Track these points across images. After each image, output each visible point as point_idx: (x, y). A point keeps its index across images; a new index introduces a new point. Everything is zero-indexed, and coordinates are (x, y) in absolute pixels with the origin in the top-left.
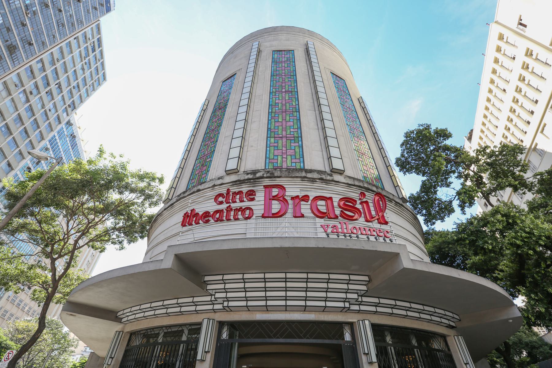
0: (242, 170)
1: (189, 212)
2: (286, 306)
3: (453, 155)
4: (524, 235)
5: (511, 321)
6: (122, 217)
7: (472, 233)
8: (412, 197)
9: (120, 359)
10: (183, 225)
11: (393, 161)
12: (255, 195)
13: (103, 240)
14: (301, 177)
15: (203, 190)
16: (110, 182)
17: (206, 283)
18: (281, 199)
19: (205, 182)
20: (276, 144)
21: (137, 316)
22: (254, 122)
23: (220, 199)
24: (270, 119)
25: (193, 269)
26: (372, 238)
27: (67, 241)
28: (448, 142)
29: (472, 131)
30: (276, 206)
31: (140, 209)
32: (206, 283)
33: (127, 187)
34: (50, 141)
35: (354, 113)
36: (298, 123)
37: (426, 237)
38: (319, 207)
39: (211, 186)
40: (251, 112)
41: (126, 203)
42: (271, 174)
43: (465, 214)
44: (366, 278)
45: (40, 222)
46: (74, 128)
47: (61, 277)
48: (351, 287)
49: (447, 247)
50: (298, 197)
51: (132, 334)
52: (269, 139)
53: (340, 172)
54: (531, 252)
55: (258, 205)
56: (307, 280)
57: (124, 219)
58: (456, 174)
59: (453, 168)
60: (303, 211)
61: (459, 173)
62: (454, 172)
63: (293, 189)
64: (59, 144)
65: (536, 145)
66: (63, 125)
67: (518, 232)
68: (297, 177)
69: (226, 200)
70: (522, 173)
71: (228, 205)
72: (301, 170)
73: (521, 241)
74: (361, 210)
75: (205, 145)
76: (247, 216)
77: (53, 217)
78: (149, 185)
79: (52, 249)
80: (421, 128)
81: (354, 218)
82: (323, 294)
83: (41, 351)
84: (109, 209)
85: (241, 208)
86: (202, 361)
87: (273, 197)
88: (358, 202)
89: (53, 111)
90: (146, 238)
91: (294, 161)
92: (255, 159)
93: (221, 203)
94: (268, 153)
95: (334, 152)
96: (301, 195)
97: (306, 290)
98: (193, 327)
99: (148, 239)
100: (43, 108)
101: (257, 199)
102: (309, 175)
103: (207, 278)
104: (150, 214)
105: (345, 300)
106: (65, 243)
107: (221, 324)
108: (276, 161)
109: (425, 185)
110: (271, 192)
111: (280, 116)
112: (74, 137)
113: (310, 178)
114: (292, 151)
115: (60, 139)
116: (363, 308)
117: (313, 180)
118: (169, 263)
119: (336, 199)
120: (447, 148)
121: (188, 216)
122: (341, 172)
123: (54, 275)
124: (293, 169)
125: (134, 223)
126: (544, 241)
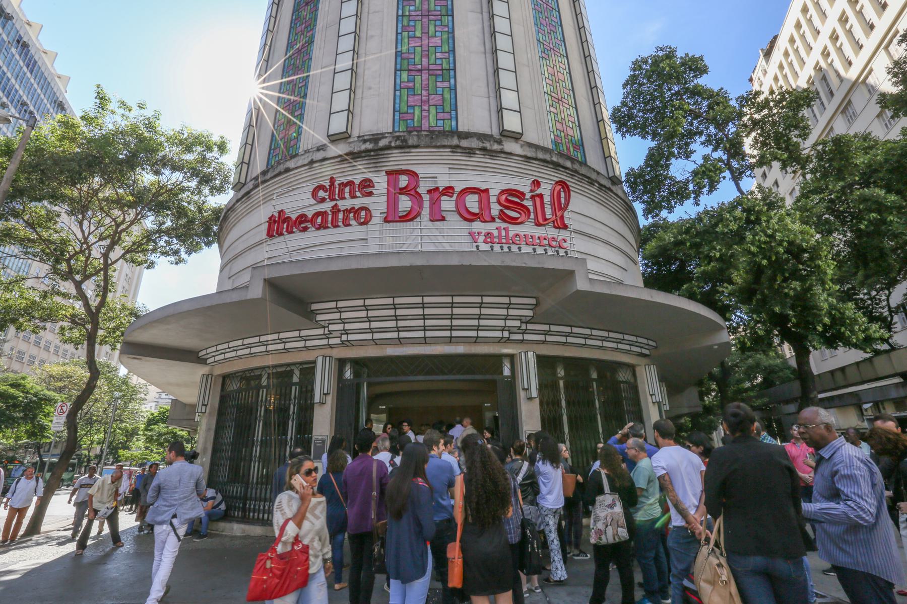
0: (355, 133)
1: (276, 215)
2: (425, 338)
3: (705, 103)
4: (763, 238)
6: (169, 212)
7: (698, 234)
9: (217, 405)
10: (270, 234)
11: (607, 114)
12: (373, 187)
13: (147, 250)
14: (450, 147)
15: (297, 168)
17: (314, 313)
18: (412, 192)
19: (296, 155)
20: (411, 84)
21: (227, 355)
22: (372, 36)
23: (321, 194)
24: (400, 31)
25: (293, 297)
26: (540, 250)
27: (90, 254)
28: (703, 81)
29: (775, 38)
30: (405, 203)
31: (196, 198)
32: (314, 313)
33: (165, 162)
35: (555, 14)
36: (451, 41)
37: (643, 238)
38: (468, 205)
39: (306, 162)
40: (365, 15)
41: (171, 190)
42: (402, 141)
43: (698, 205)
44: (533, 301)
45: (31, 225)
46: (18, 26)
47: (98, 309)
48: (511, 312)
50: (437, 188)
51: (225, 378)
52: (398, 73)
53: (515, 135)
54: (765, 262)
55: (377, 204)
57: (173, 214)
58: (703, 138)
59: (701, 128)
61: (709, 135)
62: (700, 134)
63: (435, 169)
65: (871, 71)
67: (757, 234)
68: (444, 147)
69: (329, 196)
70: (800, 140)
71: (333, 203)
73: (758, 247)
76: (362, 220)
77: (51, 217)
78: (204, 158)
79: (69, 266)
80: (661, 53)
81: (519, 220)
82: (475, 322)
83: (96, 400)
85: (353, 208)
86: (322, 403)
87: (401, 189)
88: (528, 196)
90: (215, 246)
91: (441, 115)
92: (376, 117)
93: (323, 200)
94: (397, 101)
95: (509, 99)
97: (452, 317)
98: (305, 366)
99: (221, 247)
102: (464, 143)
103: (314, 307)
104: (215, 206)
105: (503, 329)
106: (87, 258)
107: (342, 363)
108: (410, 117)
109: (653, 155)
110: (396, 181)
111: (419, 24)
112: (25, 46)
113: (465, 148)
114: (438, 98)
116: (527, 337)
117: (470, 152)
118: (257, 291)
119: (494, 193)
120: (696, 92)
121: (275, 221)
122: (516, 137)
123: (87, 305)
124: (439, 132)
125: (191, 221)
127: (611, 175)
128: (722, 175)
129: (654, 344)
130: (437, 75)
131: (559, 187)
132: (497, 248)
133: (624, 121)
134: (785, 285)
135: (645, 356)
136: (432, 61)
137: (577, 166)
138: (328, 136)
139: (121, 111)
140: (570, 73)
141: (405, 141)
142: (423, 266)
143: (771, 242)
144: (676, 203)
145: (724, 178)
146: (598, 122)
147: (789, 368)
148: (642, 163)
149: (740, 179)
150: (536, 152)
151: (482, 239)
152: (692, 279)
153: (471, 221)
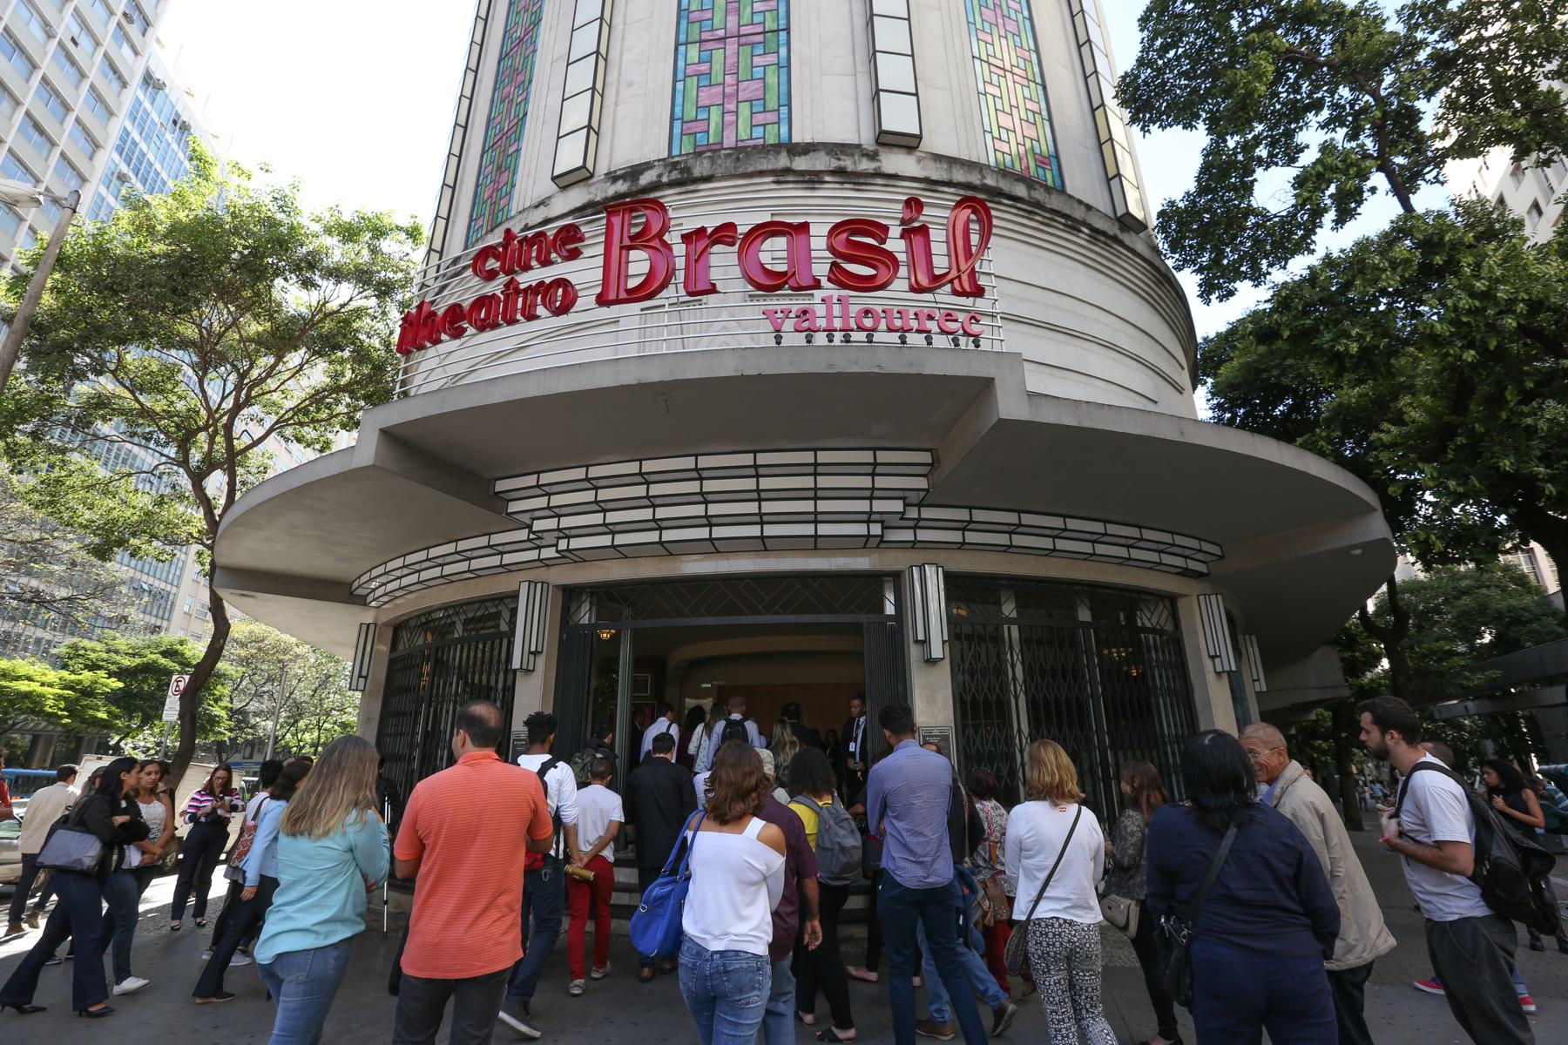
3: (1328, 39)
4: (1465, 302)
5: (1358, 552)
8: (1168, 215)
14: (773, 172)
16: (256, 253)
17: (502, 499)
20: (704, 67)
23: (492, 264)
32: (502, 499)
34: (120, 150)
42: (682, 171)
44: (926, 457)
48: (881, 482)
49: (1276, 366)
52: (682, 48)
53: (905, 141)
55: (585, 272)
56: (757, 472)
58: (1325, 114)
60: (714, 275)
61: (1335, 106)
62: (1317, 106)
64: (150, 157)
66: (135, 89)
68: (762, 173)
72: (777, 148)
74: (902, 257)
75: (502, 101)
84: (287, 336)
86: (528, 672)
89: (84, 41)
93: (491, 276)
94: (679, 100)
95: (894, 72)
96: (711, 223)
100: (50, 36)
101: (587, 252)
102: (801, 163)
103: (501, 486)
107: (570, 594)
112: (185, 128)
115: (147, 139)
116: (923, 535)
117: (812, 179)
119: (819, 232)
122: (909, 143)
124: (755, 147)
126: (1518, 316)
127: (1120, 212)
128: (1369, 184)
129: (1216, 550)
130: (753, 44)
131: (966, 213)
132: (820, 339)
133: (1146, 100)
134: (1526, 409)
135: (1199, 575)
136: (745, 19)
137: (1039, 195)
138: (554, 179)
139: (234, 180)
140: (1031, 19)
141: (688, 170)
142: (662, 383)
143: (1485, 309)
144: (1271, 265)
145: (1373, 190)
146: (1093, 110)
147: (1555, 613)
148: (1192, 186)
149: (1414, 189)
150: (950, 171)
151: (788, 325)
152: (1316, 423)
153: (770, 289)
